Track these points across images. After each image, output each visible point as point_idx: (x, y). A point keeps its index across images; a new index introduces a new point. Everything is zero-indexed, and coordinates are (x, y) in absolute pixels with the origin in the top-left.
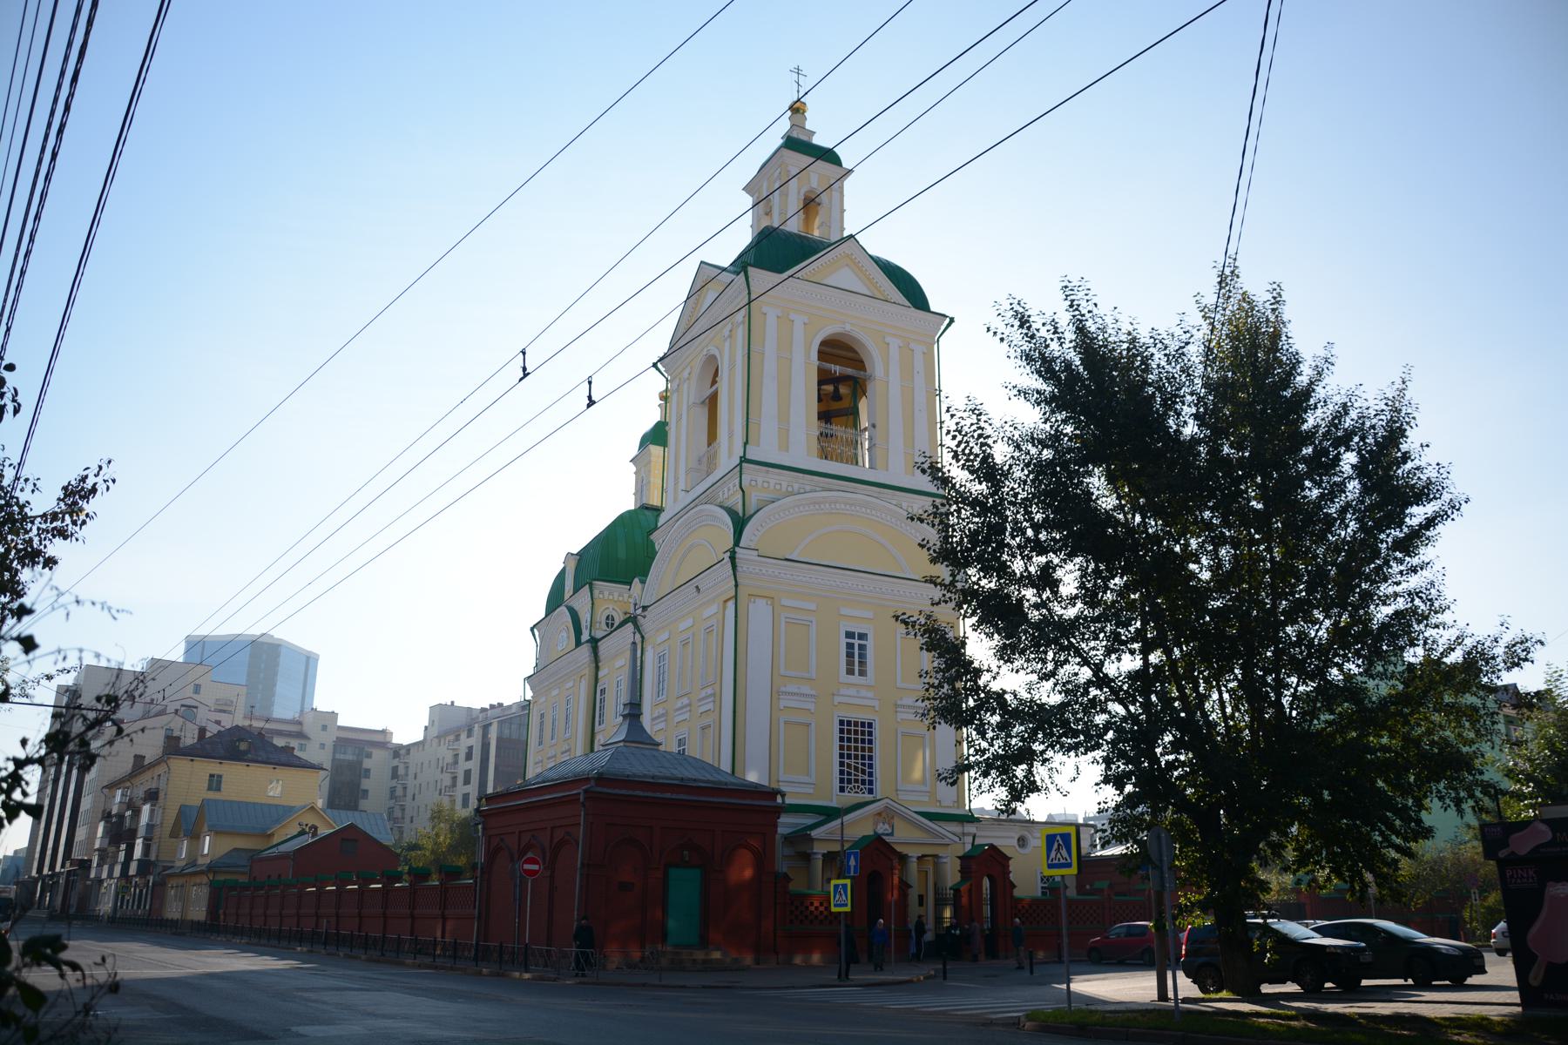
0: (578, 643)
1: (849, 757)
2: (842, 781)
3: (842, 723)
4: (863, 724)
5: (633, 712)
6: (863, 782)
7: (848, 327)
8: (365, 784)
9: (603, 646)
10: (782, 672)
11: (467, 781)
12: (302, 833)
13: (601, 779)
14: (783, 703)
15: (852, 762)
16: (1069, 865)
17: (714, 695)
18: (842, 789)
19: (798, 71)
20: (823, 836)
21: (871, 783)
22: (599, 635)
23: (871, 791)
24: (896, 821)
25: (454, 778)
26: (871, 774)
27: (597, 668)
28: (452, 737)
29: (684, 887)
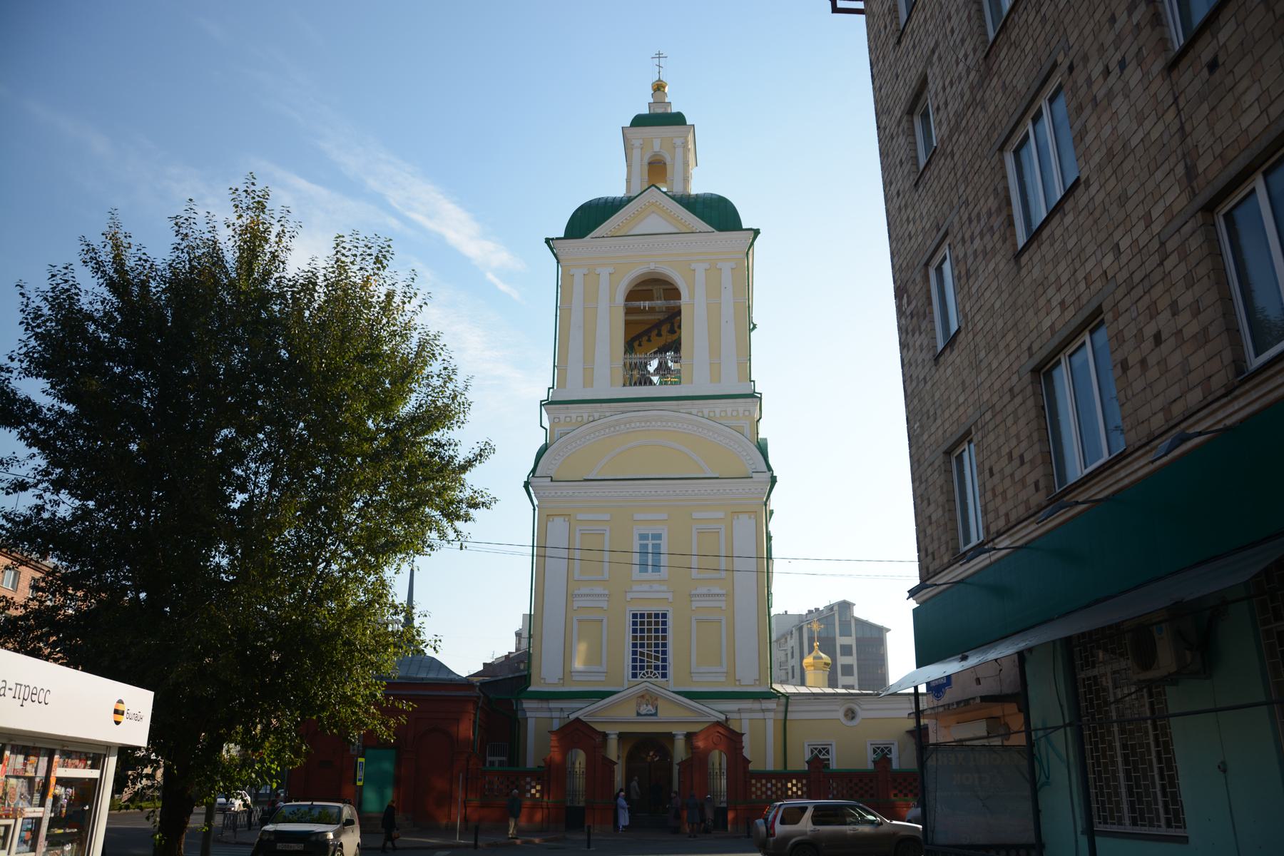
1: (642, 646)
2: (634, 668)
3: (635, 616)
4: (657, 616)
6: (657, 668)
7: (652, 266)
15: (645, 650)
18: (634, 675)
19: (659, 56)
21: (664, 668)
23: (664, 675)
24: (660, 703)
26: (664, 660)
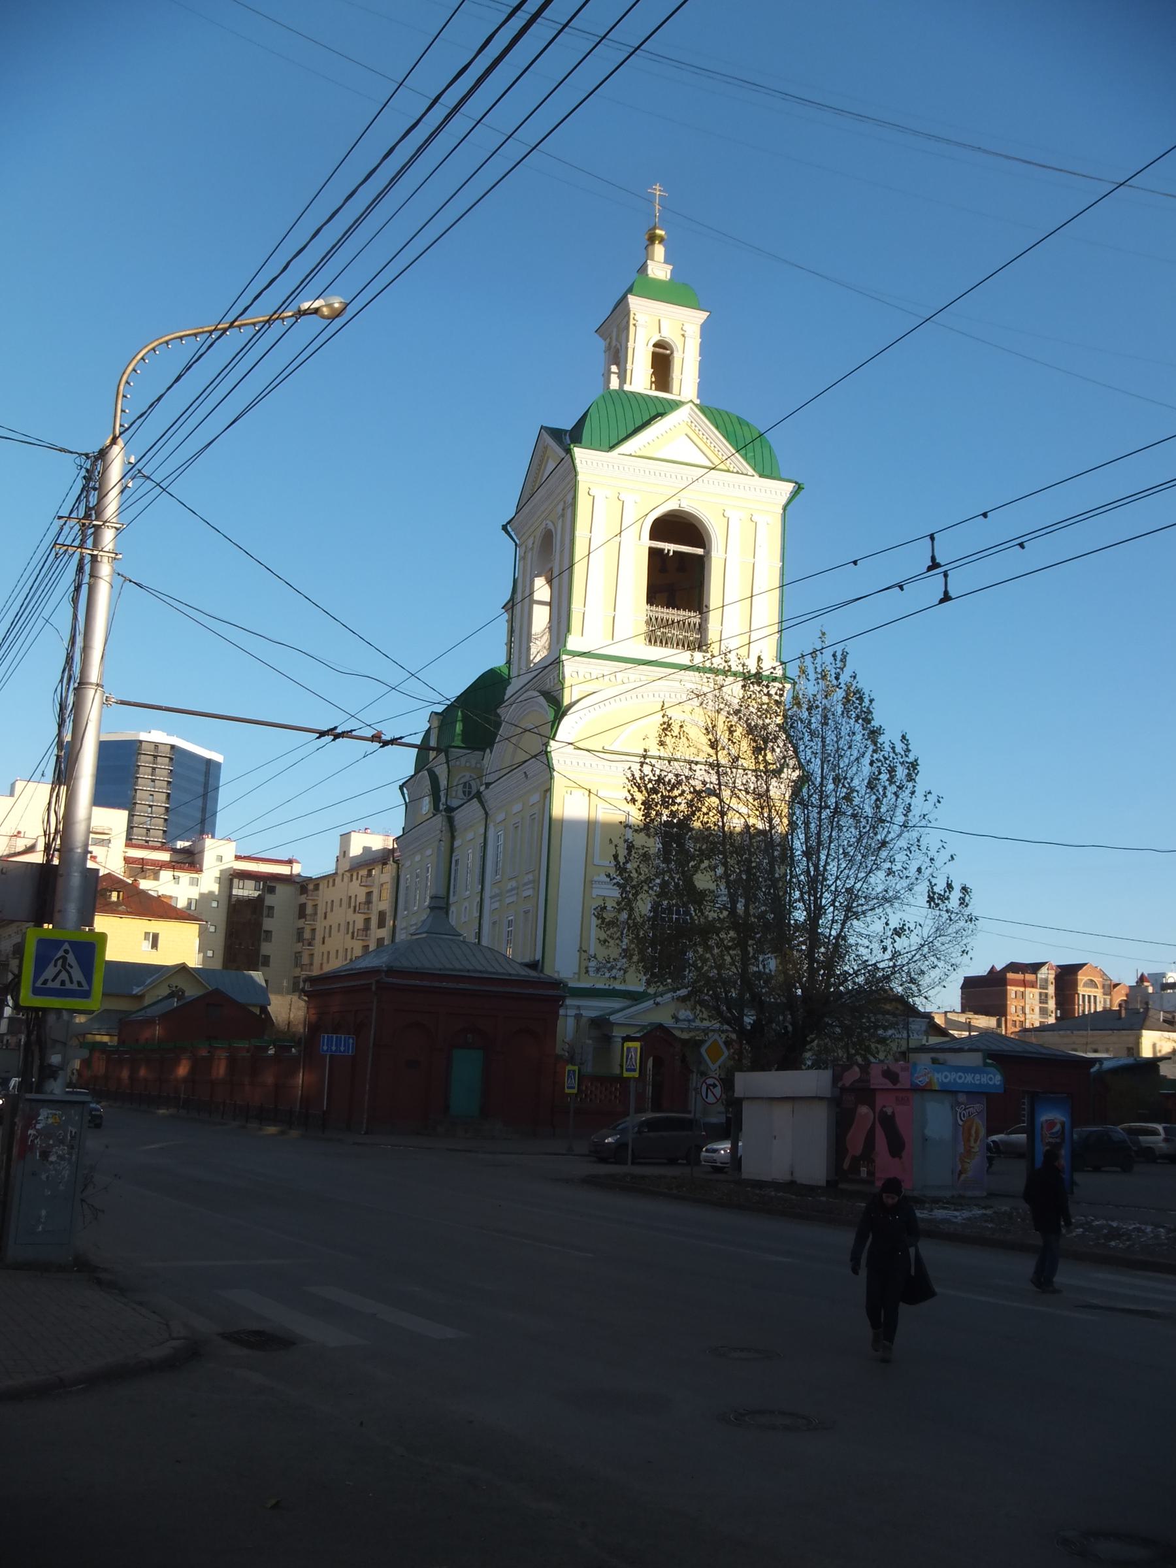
0: (436, 808)
5: (441, 905)
8: (268, 924)
9: (458, 816)
10: (597, 861)
11: (381, 925)
12: (171, 995)
13: (391, 971)
14: (595, 892)
16: (634, 1070)
17: (533, 882)
20: (622, 1021)
22: (454, 803)
25: (367, 921)
27: (453, 838)
28: (364, 872)
29: (466, 1069)
